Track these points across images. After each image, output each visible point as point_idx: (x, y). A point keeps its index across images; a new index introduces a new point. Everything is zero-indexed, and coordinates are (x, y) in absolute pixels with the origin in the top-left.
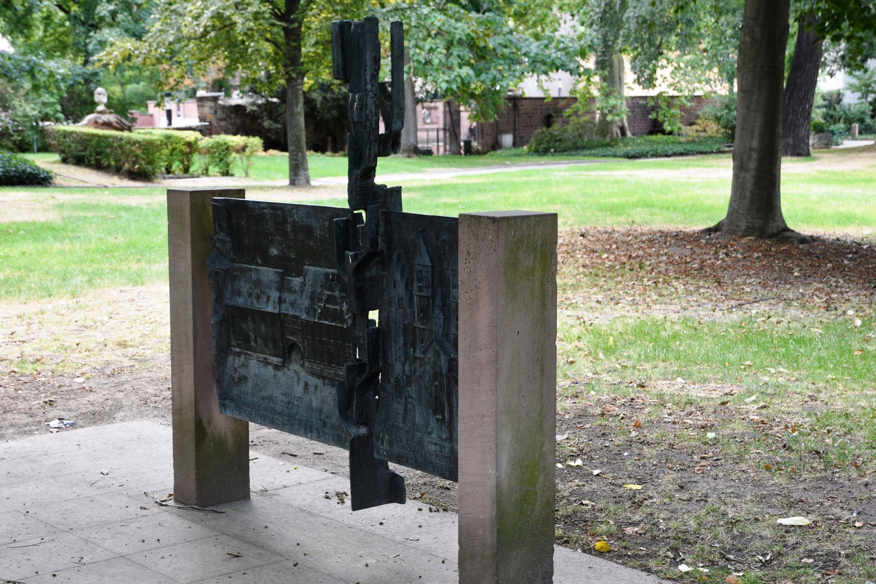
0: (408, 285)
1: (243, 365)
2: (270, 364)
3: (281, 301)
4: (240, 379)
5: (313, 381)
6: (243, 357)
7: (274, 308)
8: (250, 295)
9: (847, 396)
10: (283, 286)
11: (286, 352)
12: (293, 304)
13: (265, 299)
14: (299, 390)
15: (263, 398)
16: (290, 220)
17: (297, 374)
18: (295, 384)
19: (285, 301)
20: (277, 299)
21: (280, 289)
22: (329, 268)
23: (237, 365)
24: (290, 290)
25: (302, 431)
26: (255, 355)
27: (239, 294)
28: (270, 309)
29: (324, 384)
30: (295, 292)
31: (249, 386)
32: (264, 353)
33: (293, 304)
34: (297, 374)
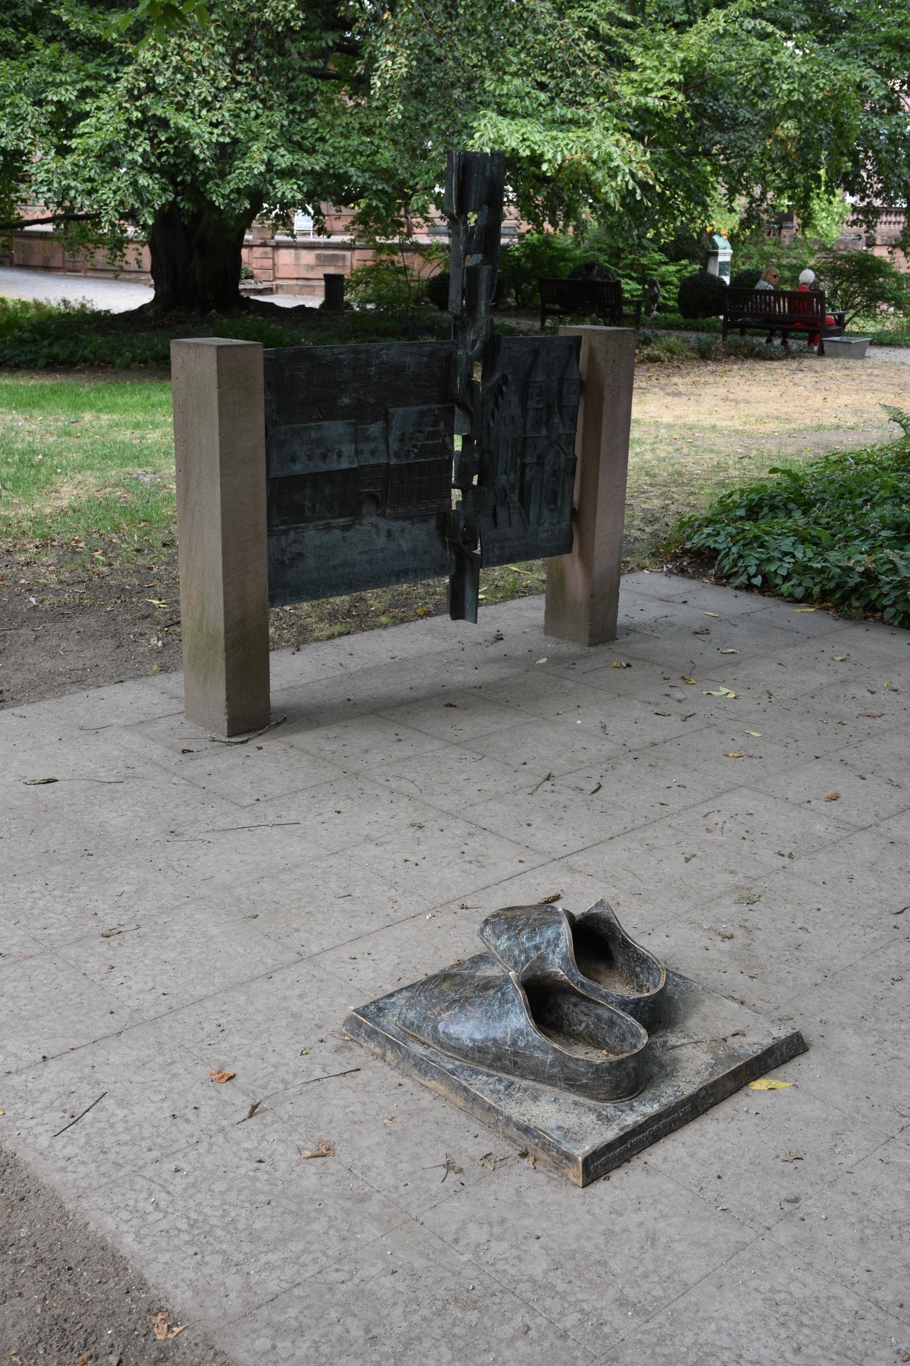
0: (523, 402)
1: (295, 542)
2: (335, 527)
3: (358, 453)
4: (293, 559)
5: (396, 525)
6: (292, 533)
7: (350, 463)
8: (310, 458)
9: (16, 419)
10: (356, 438)
11: (351, 509)
12: (373, 453)
13: (335, 457)
14: (381, 541)
15: (335, 567)
16: (375, 361)
17: (375, 526)
18: (375, 537)
19: (362, 452)
20: (353, 453)
21: (355, 441)
22: (424, 403)
23: (284, 545)
24: (367, 439)
25: (393, 580)
26: (311, 525)
27: (293, 459)
28: (344, 465)
29: (413, 524)
30: (375, 438)
31: (310, 561)
32: (325, 519)
33: (373, 453)
34: (375, 526)
